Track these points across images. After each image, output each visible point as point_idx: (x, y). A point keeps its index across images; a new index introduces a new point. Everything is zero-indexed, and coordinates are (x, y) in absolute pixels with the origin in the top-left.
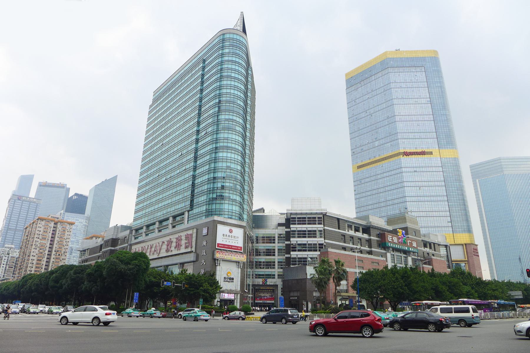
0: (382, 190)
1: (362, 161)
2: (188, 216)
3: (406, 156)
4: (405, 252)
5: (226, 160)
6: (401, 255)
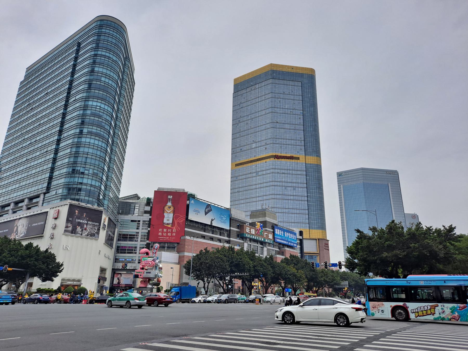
2: (44, 198)
3: (277, 159)
4: (262, 243)
5: (88, 146)
6: (258, 245)
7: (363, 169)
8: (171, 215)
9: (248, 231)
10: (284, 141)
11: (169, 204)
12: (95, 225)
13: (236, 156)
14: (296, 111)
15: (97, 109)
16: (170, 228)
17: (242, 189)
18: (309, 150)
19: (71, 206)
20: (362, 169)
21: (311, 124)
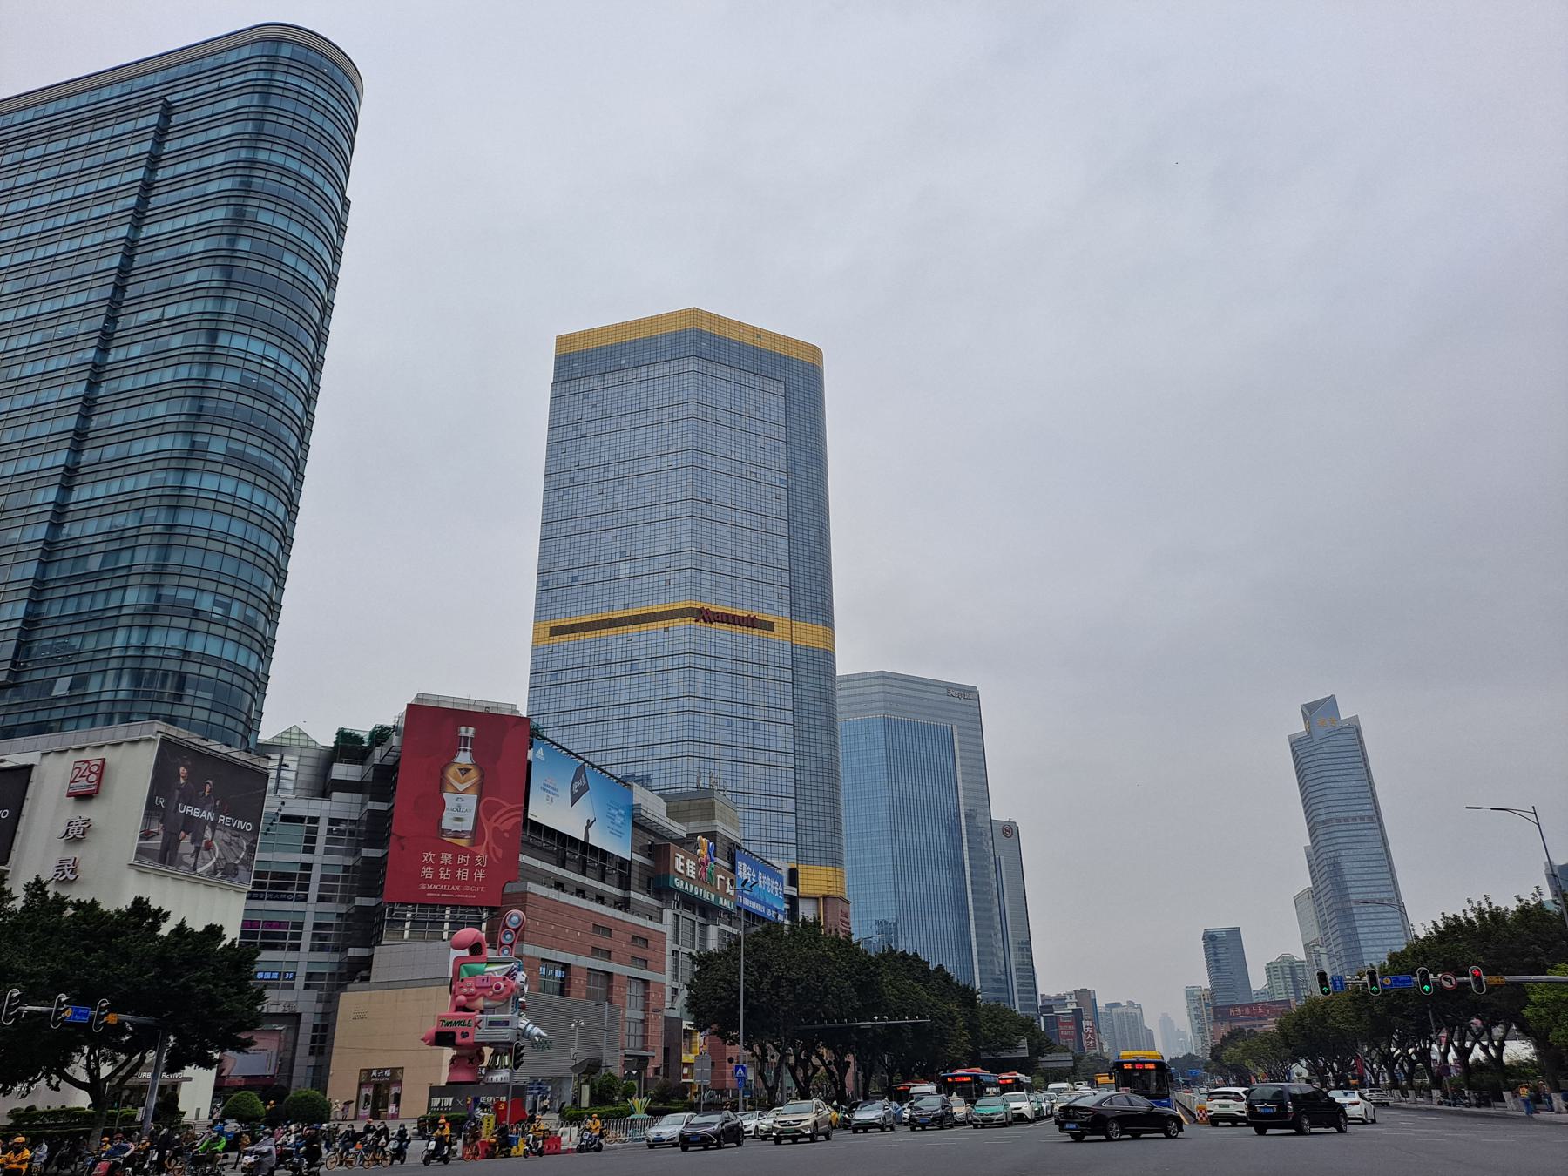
0: (616, 713)
1: (626, 607)
3: (705, 621)
5: (228, 509)
7: (884, 675)
8: (471, 801)
9: (679, 865)
10: (729, 564)
11: (464, 758)
12: (240, 830)
13: (554, 599)
14: (768, 472)
15: (265, 371)
16: (463, 850)
17: (575, 717)
18: (802, 602)
19: (166, 743)
20: (883, 677)
21: (811, 522)
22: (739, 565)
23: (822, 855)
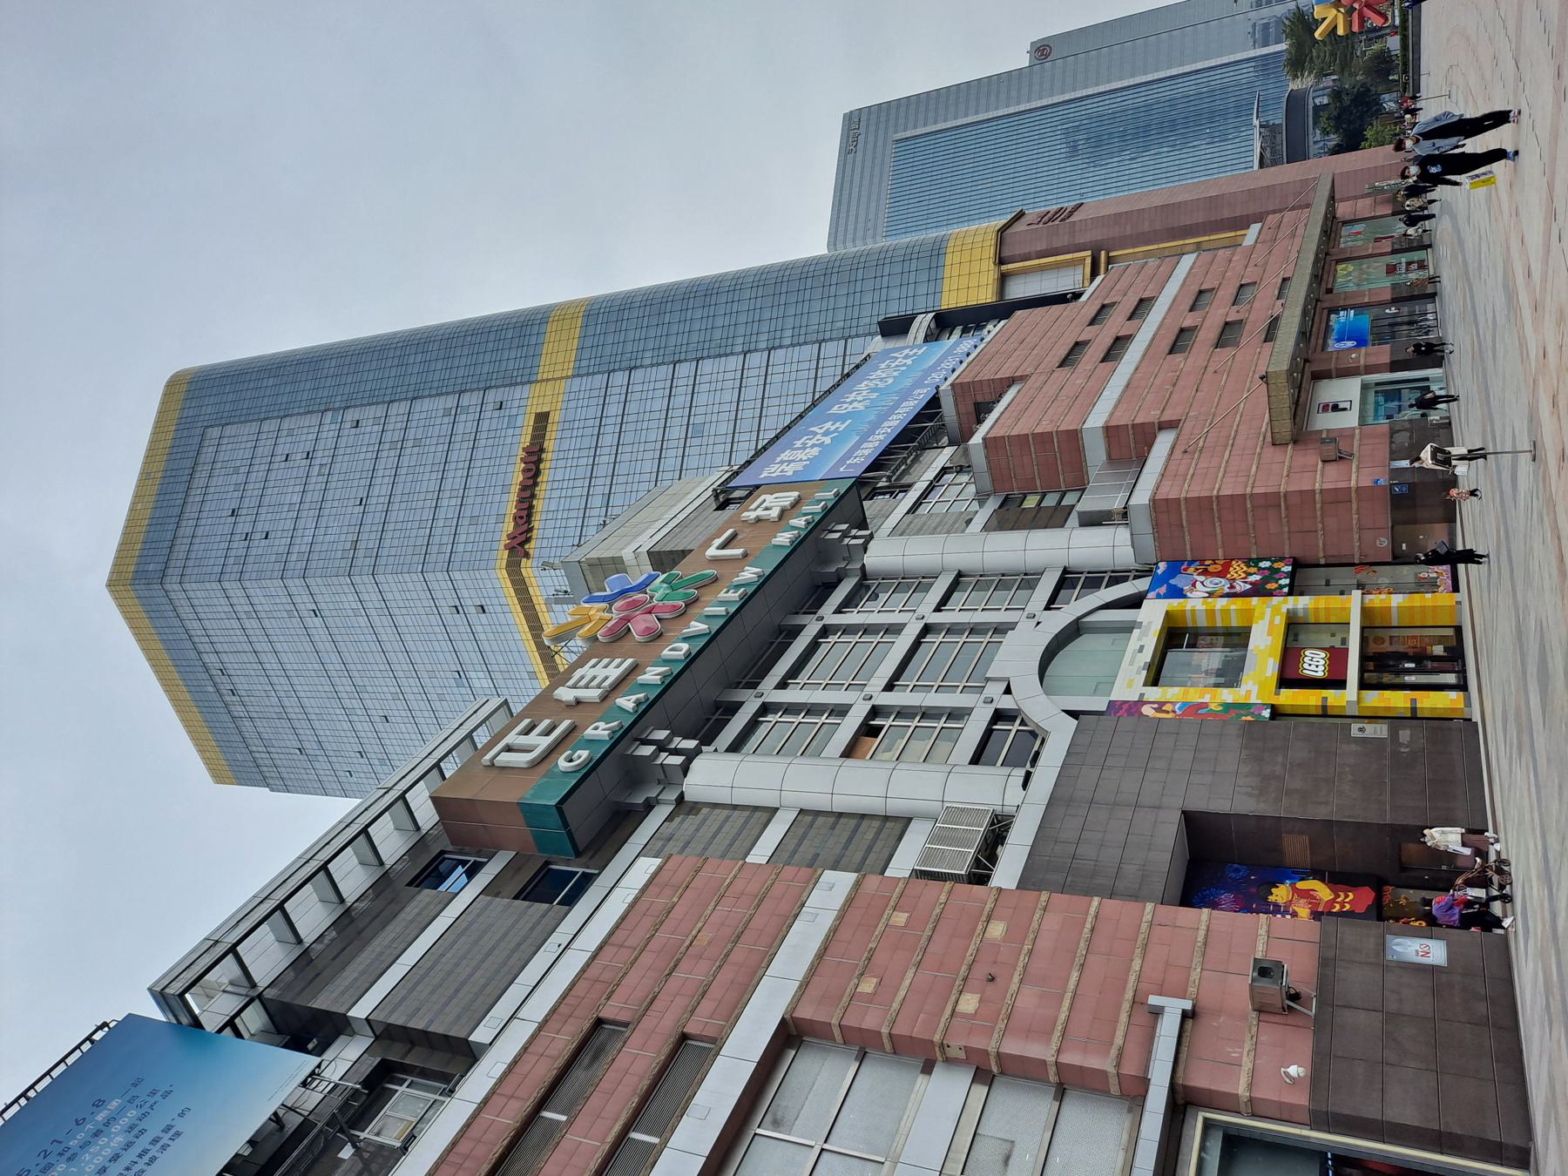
20: (835, 245)
22: (447, 485)
23: (924, 276)
